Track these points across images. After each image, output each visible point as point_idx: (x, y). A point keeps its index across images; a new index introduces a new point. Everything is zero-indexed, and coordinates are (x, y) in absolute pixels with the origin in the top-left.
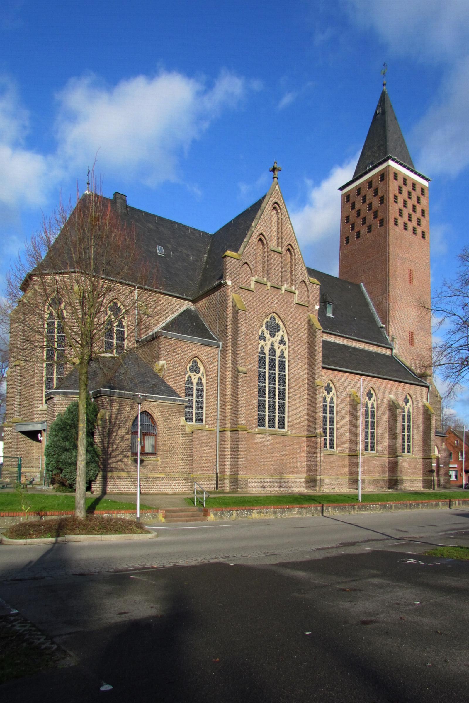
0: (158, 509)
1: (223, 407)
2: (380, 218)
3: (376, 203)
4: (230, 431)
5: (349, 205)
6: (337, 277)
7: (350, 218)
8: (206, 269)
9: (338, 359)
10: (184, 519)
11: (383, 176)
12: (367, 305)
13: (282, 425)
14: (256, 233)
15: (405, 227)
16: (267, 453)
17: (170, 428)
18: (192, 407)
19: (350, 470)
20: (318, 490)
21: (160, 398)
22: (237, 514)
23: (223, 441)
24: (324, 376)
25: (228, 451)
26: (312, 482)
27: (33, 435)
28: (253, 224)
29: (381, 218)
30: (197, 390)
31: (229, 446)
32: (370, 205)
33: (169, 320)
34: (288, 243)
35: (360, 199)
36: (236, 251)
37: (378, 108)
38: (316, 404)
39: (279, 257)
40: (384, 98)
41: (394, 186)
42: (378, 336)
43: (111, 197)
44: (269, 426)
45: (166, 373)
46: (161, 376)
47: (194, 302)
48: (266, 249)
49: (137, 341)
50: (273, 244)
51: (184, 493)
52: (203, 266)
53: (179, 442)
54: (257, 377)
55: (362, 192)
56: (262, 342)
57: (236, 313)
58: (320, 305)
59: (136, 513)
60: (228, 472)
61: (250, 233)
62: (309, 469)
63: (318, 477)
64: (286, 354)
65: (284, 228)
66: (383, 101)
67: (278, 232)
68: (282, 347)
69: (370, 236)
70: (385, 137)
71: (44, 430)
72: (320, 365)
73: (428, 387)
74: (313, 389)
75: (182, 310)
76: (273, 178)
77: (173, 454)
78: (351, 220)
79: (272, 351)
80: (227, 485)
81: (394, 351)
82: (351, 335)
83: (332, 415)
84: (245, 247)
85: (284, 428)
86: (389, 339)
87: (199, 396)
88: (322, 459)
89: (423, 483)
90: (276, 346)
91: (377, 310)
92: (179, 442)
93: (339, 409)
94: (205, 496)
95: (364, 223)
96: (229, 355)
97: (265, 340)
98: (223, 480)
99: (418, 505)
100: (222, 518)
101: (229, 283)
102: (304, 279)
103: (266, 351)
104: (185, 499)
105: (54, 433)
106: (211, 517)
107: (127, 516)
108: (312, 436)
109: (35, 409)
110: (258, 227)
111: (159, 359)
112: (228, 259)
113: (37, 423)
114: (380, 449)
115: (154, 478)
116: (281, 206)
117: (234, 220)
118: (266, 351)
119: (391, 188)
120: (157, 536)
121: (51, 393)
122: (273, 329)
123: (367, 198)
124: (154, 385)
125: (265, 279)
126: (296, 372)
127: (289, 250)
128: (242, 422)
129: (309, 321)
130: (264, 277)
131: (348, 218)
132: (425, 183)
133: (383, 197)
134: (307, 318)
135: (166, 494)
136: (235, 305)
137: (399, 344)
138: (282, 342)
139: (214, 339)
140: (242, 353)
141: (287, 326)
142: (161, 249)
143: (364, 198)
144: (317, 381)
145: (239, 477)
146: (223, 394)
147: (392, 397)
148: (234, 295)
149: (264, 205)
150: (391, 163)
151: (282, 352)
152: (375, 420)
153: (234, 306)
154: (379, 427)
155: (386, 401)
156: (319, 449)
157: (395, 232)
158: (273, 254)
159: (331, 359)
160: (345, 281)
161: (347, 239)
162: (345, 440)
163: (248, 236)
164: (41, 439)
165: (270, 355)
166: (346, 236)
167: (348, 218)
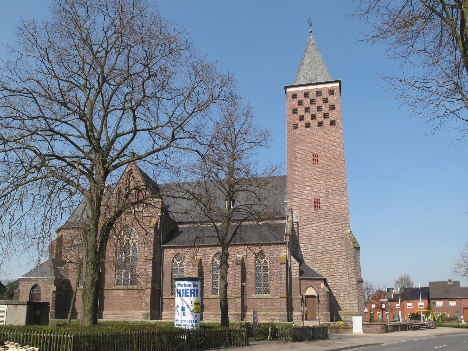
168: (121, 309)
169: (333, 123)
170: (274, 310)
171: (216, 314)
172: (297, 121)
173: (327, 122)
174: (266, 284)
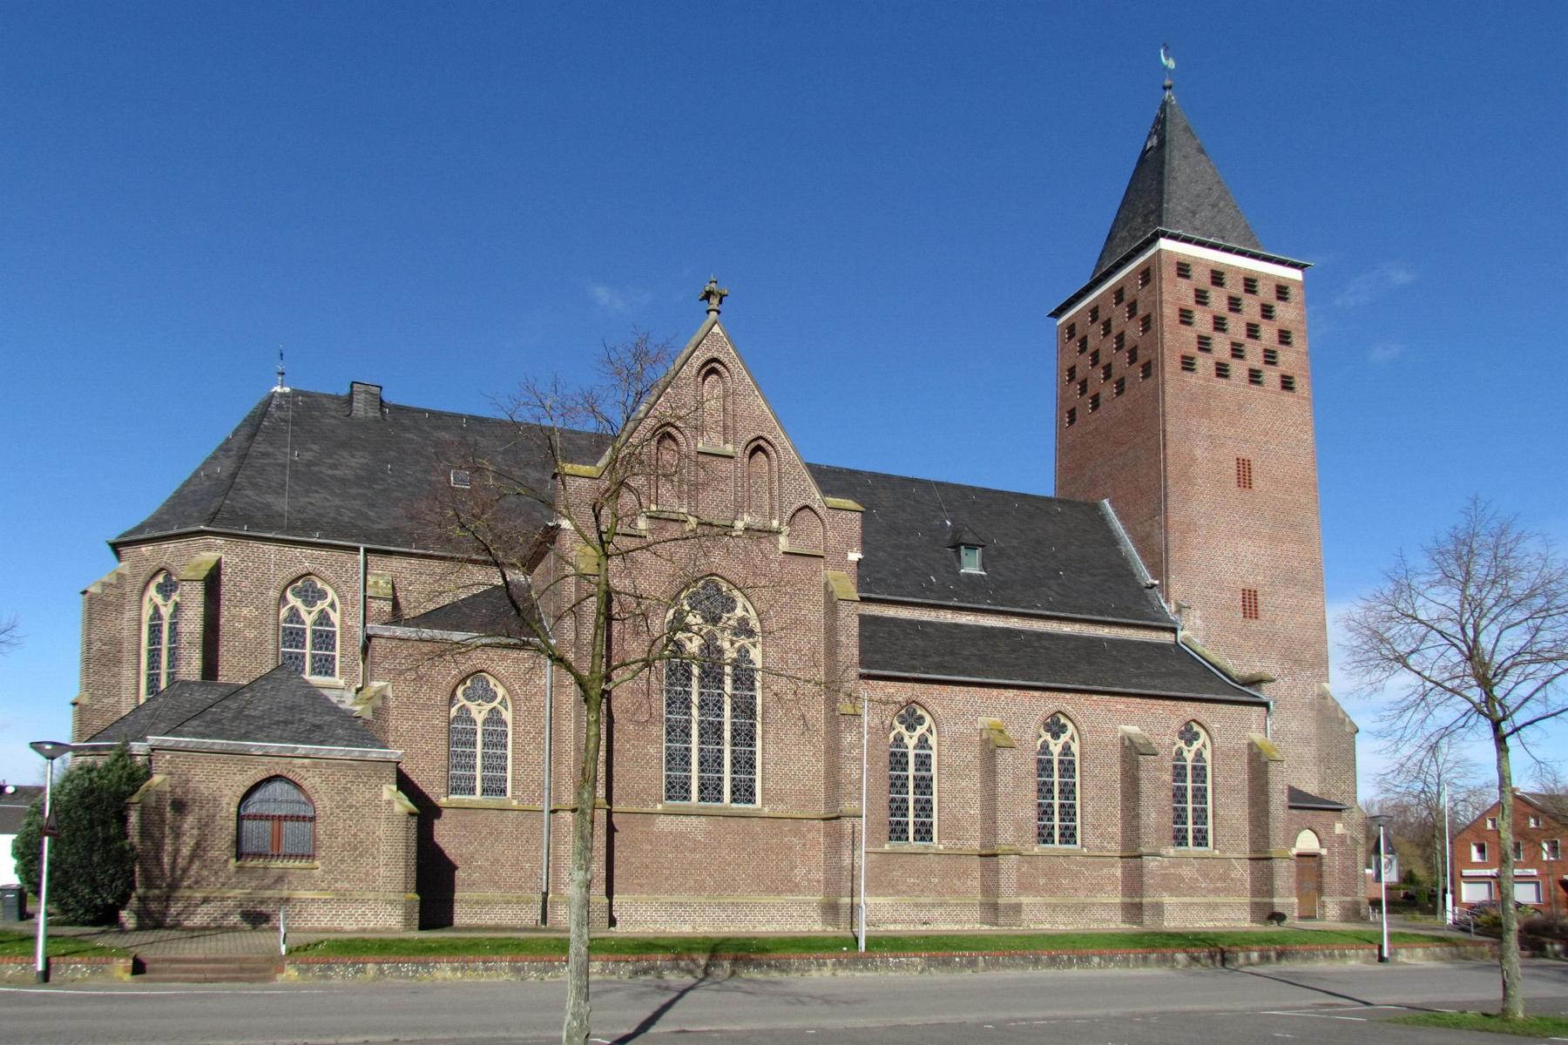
2: (1142, 360)
3: (1133, 331)
5: (1075, 344)
11: (1146, 275)
12: (1112, 541)
13: (744, 792)
15: (1222, 371)
17: (351, 807)
18: (473, 767)
19: (983, 885)
26: (1134, 910)
29: (1145, 360)
32: (1120, 338)
35: (1098, 328)
37: (1150, 137)
41: (1175, 293)
42: (1137, 605)
55: (1101, 313)
58: (865, 545)
59: (35, 961)
68: (743, 641)
70: (1161, 192)
72: (853, 673)
73: (1266, 705)
77: (361, 855)
78: (1079, 375)
79: (711, 647)
83: (923, 773)
86: (1170, 609)
87: (495, 745)
89: (1253, 912)
91: (1140, 552)
95: (1107, 376)
101: (566, 524)
102: (808, 502)
119: (1166, 296)
123: (1113, 323)
131: (1072, 371)
132: (1296, 275)
133: (1148, 316)
143: (1107, 326)
147: (1132, 729)
150: (1164, 244)
159: (936, 659)
167: (1072, 371)
168: (700, 888)
169: (1287, 383)
170: (1227, 891)
171: (1056, 905)
172: (1192, 349)
173: (1271, 376)
174: (923, 809)
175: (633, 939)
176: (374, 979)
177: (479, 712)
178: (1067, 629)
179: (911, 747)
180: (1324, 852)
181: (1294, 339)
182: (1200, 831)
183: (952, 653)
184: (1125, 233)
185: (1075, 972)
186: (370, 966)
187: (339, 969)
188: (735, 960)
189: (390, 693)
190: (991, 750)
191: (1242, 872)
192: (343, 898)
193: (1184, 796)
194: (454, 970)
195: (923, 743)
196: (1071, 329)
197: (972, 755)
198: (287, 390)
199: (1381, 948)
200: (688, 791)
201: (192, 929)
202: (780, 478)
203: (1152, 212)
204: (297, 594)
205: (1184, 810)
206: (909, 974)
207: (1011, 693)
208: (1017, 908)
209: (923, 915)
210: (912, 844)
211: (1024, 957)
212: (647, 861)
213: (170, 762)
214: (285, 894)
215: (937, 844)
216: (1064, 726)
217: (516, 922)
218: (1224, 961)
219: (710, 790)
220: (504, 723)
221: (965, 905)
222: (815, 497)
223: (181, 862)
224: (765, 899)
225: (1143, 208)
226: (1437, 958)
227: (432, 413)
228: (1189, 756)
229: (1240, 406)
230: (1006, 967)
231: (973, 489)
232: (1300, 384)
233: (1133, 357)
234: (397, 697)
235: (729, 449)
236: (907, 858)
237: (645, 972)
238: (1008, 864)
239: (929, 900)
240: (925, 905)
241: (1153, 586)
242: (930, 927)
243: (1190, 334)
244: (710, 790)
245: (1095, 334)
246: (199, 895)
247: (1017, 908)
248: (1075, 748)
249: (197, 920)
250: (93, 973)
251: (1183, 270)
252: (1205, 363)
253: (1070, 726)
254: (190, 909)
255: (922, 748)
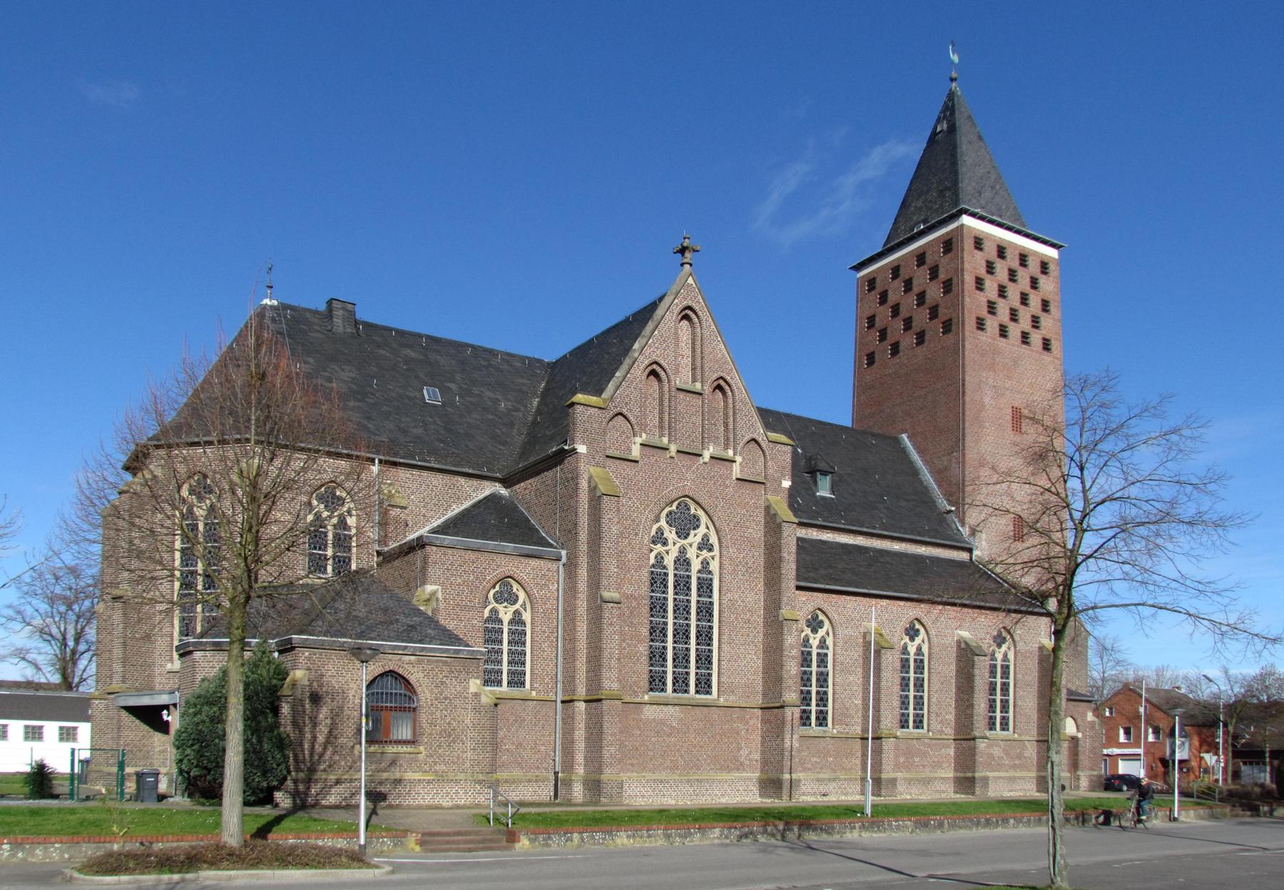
0: (405, 832)
1: (570, 657)
3: (935, 293)
4: (585, 701)
5: (875, 296)
6: (847, 422)
7: (877, 319)
8: (535, 423)
9: (826, 572)
10: (462, 846)
11: (949, 245)
12: (915, 473)
13: (704, 685)
14: (643, 362)
15: (1003, 332)
16: (670, 735)
17: (446, 698)
20: (785, 797)
21: (423, 649)
22: (582, 839)
23: (569, 721)
24: (800, 605)
25: (580, 734)
27: (151, 716)
28: (636, 346)
30: (511, 632)
31: (582, 725)
33: (450, 514)
34: (715, 376)
36: (598, 392)
37: (939, 121)
38: (782, 650)
39: (697, 401)
40: (953, 105)
41: (973, 263)
43: (322, 307)
44: (675, 691)
45: (442, 606)
46: (430, 613)
47: (507, 482)
48: (666, 388)
49: (379, 553)
50: (683, 378)
51: (478, 806)
52: (530, 419)
53: (468, 721)
54: (647, 608)
55: (902, 271)
56: (659, 548)
57: (596, 500)
58: (794, 478)
59: (358, 837)
60: (580, 770)
61: (628, 361)
62: (765, 763)
63: (787, 776)
64: (714, 566)
65: (707, 351)
66: (949, 110)
67: (693, 357)
68: (705, 553)
69: (921, 351)
70: (956, 173)
71: (175, 705)
72: (793, 584)
74: (775, 625)
75: (481, 497)
76: (682, 265)
77: (454, 741)
78: (879, 323)
79: (683, 562)
80: (578, 792)
81: (976, 553)
82: (874, 528)
83: (822, 669)
84: (618, 388)
85: (709, 693)
86: (965, 531)
87: (516, 643)
88: (796, 744)
90: (692, 553)
92: (468, 721)
93: (840, 658)
94: (510, 810)
96: (583, 573)
97: (665, 543)
98: (568, 783)
99: (1005, 821)
100: (548, 845)
101: (582, 449)
102: (755, 436)
103: (669, 561)
104: (475, 815)
105: (191, 711)
106: (524, 843)
107: (341, 843)
108: (772, 708)
109: (157, 671)
110: (647, 351)
111: (424, 583)
112: (579, 409)
113: (161, 693)
114: (936, 726)
115: (411, 782)
116: (700, 313)
117: (597, 337)
118: (669, 561)
119: (966, 266)
120: (393, 872)
121: (188, 644)
122: (685, 524)
123: (915, 282)
124: (413, 627)
125: (665, 440)
126: (739, 599)
127: (719, 387)
128: (610, 683)
129: (768, 508)
130: (662, 435)
132: (1052, 253)
133: (950, 280)
134: (762, 503)
135: (458, 807)
136: (595, 487)
137: (988, 541)
138: (705, 545)
139: (551, 546)
140: (610, 566)
141: (715, 519)
142: (434, 392)
143: (908, 285)
144: (785, 612)
145: (604, 777)
146: (570, 638)
147: (965, 634)
148: (592, 469)
149: (659, 312)
150: (966, 220)
151: (705, 564)
152: (926, 675)
153: (593, 489)
154: (934, 688)
155: (951, 641)
156: (788, 728)
157: (976, 343)
158: (682, 395)
159: (823, 572)
160: (864, 433)
161: (871, 358)
162: (853, 712)
163: (624, 367)
164: (170, 719)
165: (676, 569)
166: (868, 352)
167: (871, 320)
168: (674, 768)
169: (1046, 345)
170: (1022, 767)
171: (912, 779)
175: (702, 809)
176: (579, 846)
177: (506, 614)
178: (897, 547)
179: (814, 647)
180: (1080, 735)
181: (1052, 308)
182: (821, 712)
183: (831, 567)
184: (920, 204)
185: (1000, 831)
186: (575, 835)
187: (555, 838)
188: (801, 826)
189: (440, 595)
190: (873, 651)
191: (1031, 751)
192: (441, 779)
193: (809, 680)
194: (628, 837)
195: (823, 644)
196: (872, 283)
197: (857, 653)
198: (275, 303)
199: (1171, 810)
200: (664, 684)
201: (327, 807)
202: (734, 413)
203: (947, 189)
204: (320, 499)
205: (809, 692)
206: (656, 841)
207: (885, 602)
208: (893, 781)
209: (823, 789)
210: (814, 729)
211: (971, 820)
212: (637, 744)
213: (309, 659)
214: (398, 776)
215: (829, 727)
216: (822, 622)
217: (535, 798)
218: (1084, 821)
219: (681, 683)
220: (524, 623)
221: (850, 780)
222: (760, 432)
223: (318, 749)
224: (724, 776)
225: (936, 185)
226: (1203, 818)
227: (397, 331)
228: (912, 649)
229: (1015, 362)
230: (961, 828)
231: (810, 421)
232: (1055, 345)
233: (934, 312)
234: (445, 599)
235: (698, 386)
236: (811, 741)
237: (746, 836)
238: (888, 745)
239: (826, 776)
240: (823, 780)
241: (950, 511)
242: (825, 799)
243: (982, 298)
244: (681, 683)
245: (896, 292)
246: (333, 777)
247: (893, 781)
248: (925, 649)
249: (332, 799)
250: (395, 845)
251: (978, 243)
252: (992, 324)
253: (827, 623)
254: (325, 791)
255: (822, 648)
